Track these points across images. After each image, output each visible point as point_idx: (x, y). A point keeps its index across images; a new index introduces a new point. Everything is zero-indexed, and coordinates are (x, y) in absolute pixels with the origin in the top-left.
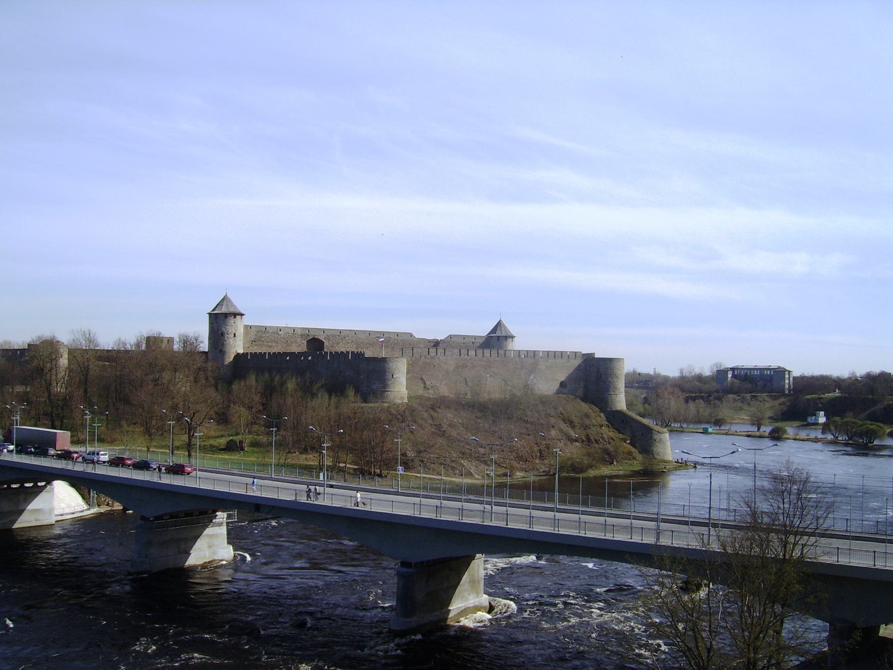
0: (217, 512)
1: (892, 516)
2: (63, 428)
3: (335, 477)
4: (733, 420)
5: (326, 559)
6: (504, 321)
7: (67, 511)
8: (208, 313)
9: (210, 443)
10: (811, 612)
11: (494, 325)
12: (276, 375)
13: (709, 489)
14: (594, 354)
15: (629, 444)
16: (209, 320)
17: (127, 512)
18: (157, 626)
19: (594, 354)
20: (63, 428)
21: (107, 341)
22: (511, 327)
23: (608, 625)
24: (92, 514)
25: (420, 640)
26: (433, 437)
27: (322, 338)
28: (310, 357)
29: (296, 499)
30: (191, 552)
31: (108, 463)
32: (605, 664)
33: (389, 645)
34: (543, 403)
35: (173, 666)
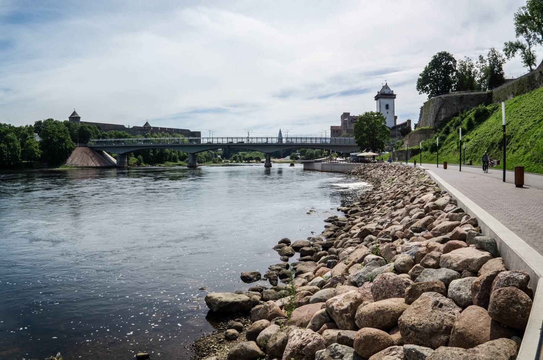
0: (179, 323)
1: (542, 132)
2: (281, 355)
3: (469, 300)
4: (377, 259)
5: (49, 225)
6: (148, 122)
7: (84, 170)
8: (275, 248)
9: (431, 304)
10: (338, 311)
11: (458, 192)
12: (481, 81)
13: (461, 167)
14: (349, 113)
15: (128, 309)
16: (156, 127)
17: (438, 146)
18: (55, 337)
19: (349, 113)
20: (281, 355)
21: (430, 61)
22: (79, 114)
23: (427, 176)
24: (165, 180)
25: (142, 156)
26: (528, 87)
27: (100, 126)
28: (181, 325)
29: (267, 141)
30: (204, 168)
31: (292, 287)
32: (444, 218)
33: (361, 230)
34: (99, 128)
35: (89, 340)
